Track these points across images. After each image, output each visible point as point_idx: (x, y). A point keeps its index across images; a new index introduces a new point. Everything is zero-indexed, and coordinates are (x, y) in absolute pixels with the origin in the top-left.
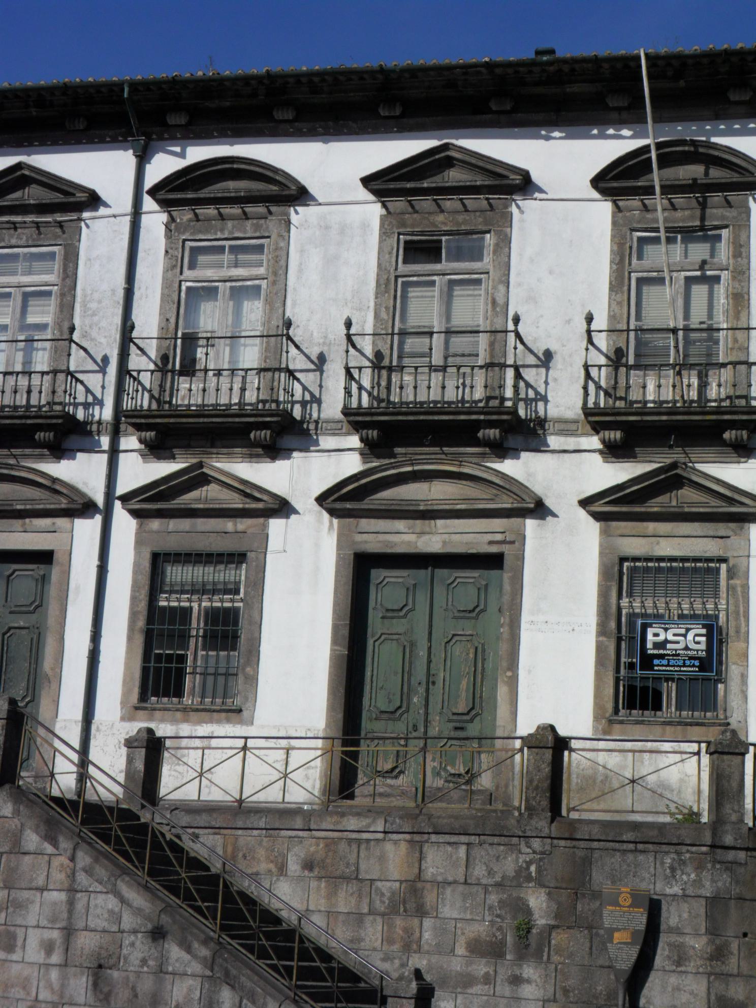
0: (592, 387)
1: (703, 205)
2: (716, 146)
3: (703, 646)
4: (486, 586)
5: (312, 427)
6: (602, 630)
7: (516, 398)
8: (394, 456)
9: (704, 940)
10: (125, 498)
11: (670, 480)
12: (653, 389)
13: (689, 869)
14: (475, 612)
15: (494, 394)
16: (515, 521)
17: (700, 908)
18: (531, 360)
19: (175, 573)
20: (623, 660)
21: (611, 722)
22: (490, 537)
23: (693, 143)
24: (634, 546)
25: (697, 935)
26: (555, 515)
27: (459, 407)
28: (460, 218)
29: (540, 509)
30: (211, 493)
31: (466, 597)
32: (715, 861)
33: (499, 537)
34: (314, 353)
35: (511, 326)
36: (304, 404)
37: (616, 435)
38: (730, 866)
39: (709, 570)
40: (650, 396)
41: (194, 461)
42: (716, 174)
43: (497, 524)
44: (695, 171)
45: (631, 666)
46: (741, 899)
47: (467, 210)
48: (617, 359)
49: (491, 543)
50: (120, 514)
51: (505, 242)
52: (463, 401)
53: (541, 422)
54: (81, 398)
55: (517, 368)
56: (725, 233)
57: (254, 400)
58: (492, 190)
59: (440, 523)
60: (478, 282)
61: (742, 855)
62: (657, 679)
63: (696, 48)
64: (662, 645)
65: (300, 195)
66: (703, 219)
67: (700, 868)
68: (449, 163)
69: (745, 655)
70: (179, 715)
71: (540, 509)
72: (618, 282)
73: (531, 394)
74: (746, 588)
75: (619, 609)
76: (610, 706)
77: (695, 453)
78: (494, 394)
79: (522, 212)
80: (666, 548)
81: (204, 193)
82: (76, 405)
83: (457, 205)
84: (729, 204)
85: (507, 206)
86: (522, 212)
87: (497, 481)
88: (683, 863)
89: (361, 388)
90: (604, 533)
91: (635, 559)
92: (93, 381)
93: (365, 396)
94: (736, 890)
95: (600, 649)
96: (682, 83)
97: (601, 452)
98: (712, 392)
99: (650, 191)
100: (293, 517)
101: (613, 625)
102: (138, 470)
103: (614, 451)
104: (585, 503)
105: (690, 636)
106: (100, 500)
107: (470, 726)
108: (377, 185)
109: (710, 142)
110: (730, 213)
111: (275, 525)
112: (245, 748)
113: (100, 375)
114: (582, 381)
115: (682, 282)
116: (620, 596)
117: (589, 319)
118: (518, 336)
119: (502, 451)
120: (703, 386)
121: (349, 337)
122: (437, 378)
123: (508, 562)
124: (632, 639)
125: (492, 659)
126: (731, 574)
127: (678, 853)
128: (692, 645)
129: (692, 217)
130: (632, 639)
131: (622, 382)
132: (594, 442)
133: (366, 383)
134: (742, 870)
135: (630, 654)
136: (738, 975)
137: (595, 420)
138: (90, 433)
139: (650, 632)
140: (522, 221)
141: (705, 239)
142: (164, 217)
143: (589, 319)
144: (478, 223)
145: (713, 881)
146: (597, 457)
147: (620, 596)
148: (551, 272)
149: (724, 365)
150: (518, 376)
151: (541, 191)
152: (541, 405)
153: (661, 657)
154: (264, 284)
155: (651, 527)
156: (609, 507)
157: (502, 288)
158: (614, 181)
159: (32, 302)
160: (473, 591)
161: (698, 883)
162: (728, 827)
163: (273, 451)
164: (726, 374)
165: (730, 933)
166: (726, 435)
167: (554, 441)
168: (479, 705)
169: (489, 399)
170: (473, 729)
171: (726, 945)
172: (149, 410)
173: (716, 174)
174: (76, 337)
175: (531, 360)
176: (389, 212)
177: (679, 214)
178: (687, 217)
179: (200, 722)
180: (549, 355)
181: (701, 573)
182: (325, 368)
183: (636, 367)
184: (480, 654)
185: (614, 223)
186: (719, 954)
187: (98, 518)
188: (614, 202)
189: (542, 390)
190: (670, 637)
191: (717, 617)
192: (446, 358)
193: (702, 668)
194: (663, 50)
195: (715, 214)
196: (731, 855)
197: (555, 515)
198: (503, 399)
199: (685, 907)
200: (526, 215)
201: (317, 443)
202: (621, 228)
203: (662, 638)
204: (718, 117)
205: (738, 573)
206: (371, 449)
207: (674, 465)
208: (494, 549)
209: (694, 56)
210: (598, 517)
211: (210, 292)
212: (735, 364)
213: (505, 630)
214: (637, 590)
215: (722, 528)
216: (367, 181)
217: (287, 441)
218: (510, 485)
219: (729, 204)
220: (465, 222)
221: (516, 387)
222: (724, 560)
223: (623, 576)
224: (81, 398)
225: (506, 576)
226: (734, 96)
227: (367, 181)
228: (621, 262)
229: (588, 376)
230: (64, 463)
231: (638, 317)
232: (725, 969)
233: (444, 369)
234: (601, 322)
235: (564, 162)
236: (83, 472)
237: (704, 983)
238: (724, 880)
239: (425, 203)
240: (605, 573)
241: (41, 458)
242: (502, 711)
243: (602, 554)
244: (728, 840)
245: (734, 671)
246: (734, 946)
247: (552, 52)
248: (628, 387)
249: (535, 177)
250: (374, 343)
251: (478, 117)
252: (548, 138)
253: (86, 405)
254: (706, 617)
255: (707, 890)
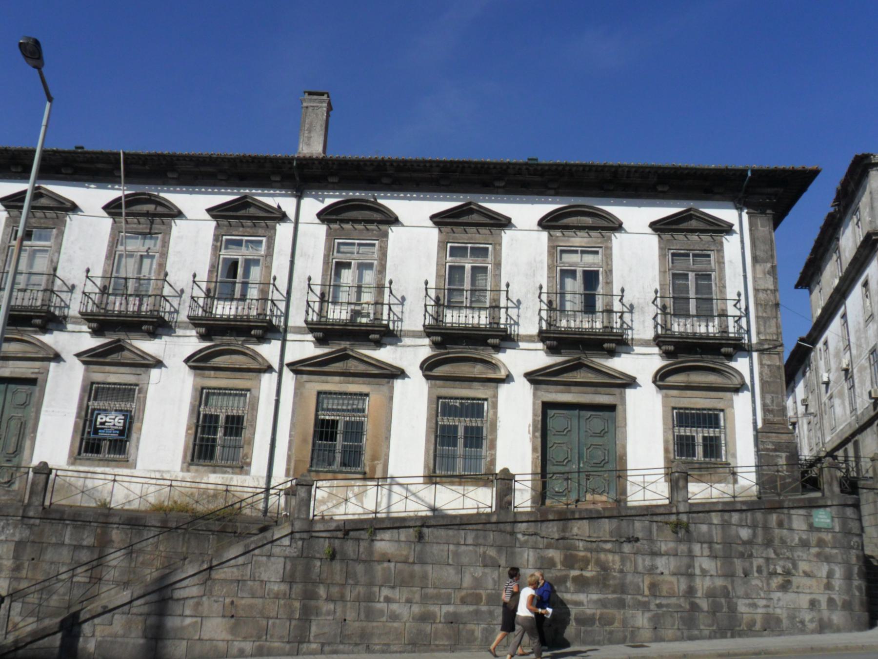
0: (427, 315)
1: (152, 223)
2: (158, 196)
3: (122, 425)
4: (31, 394)
5: (173, 325)
6: (78, 416)
7: (389, 320)
8: (446, 349)
9: (11, 561)
10: (288, 365)
11: (117, 347)
12: (117, 305)
13: (10, 527)
14: (24, 405)
15: (608, 328)
16: (46, 363)
17: (12, 546)
18: (65, 289)
19: (328, 403)
20: (199, 435)
21: (76, 459)
22: (32, 370)
23: (149, 195)
24: (98, 377)
25: (8, 559)
26: (64, 361)
27: (592, 333)
28: (42, 221)
29: (57, 358)
30: (353, 366)
31: (21, 398)
32: (23, 524)
33: (36, 370)
34: (178, 290)
35: (272, 282)
36: (394, 322)
37: (438, 339)
38: (31, 527)
39: (241, 395)
40: (116, 309)
41: (577, 356)
42: (160, 209)
43: (38, 364)
44: (150, 208)
45: (89, 433)
46: (33, 542)
47: (46, 217)
48: (104, 291)
49: (33, 373)
50: (286, 371)
51: (61, 233)
52: (592, 328)
53: (65, 318)
54: (168, 309)
55: (389, 305)
56: (160, 236)
57: (255, 313)
58: (492, 225)
59: (11, 362)
60: (47, 251)
61: (37, 521)
62: (100, 440)
63: (146, 152)
64: (103, 424)
65: (179, 214)
66: (151, 229)
67: (15, 527)
68: (471, 211)
69: (140, 429)
70: (96, 462)
71: (57, 358)
72: (111, 254)
73: (396, 318)
74: (145, 398)
75: (88, 406)
76: (76, 451)
77: (132, 335)
78: (608, 328)
79: (71, 220)
80: (112, 379)
81: (461, 220)
82: (165, 312)
83: (136, 220)
84: (163, 223)
85: (64, 217)
86: (71, 220)
87: (38, 344)
88: (8, 525)
89: (314, 311)
90: (86, 370)
91: (98, 383)
92: (175, 302)
93: (315, 315)
94: (32, 538)
95: (76, 424)
96: (147, 167)
97: (90, 333)
98: (144, 308)
99: (120, 214)
100: (406, 379)
101: (83, 413)
102: (90, 342)
103: (96, 332)
104: (78, 355)
105: (116, 420)
106: (276, 366)
107: (14, 460)
108: (214, 213)
109: (375, 202)
110: (163, 227)
111: (629, 392)
112: (114, 481)
113: (516, 310)
114: (423, 313)
115: (138, 257)
116: (89, 400)
117: (426, 283)
118: (274, 285)
119: (44, 330)
120: (141, 305)
121: (309, 285)
122: (20, 294)
123: (39, 382)
124: (91, 421)
125: (26, 429)
126: (139, 392)
127: (7, 520)
128: (117, 424)
129: (146, 228)
130: (91, 421)
131: (104, 301)
132: (194, 333)
133: (201, 304)
134: (36, 528)
135: (90, 427)
136: (26, 578)
137: (543, 336)
138: (171, 327)
139: (99, 417)
140: (70, 224)
141: (151, 238)
142: (214, 223)
143: (426, 283)
144: (50, 223)
145: (20, 533)
146: (88, 335)
147: (89, 400)
148: (80, 249)
149: (150, 296)
150: (390, 309)
151: (82, 211)
152: (66, 310)
153: (102, 429)
154: (375, 262)
155: (107, 368)
156: (535, 378)
157: (56, 255)
158: (112, 208)
159: (38, 255)
160: (24, 395)
161: (13, 534)
162: (32, 508)
163: (153, 335)
164: (151, 299)
165: (25, 558)
166: (253, 332)
167: (70, 327)
168: (18, 450)
169: (259, 315)
170: (15, 461)
171: (22, 564)
172: (92, 311)
173: (160, 209)
174: (167, 279)
175: (65, 289)
176: (10, 216)
177: (141, 226)
178: (144, 228)
179: (98, 466)
180: (403, 298)
181: (475, 409)
182: (405, 303)
183: (113, 294)
184: (23, 425)
185: (112, 228)
186: (17, 568)
187: (275, 375)
188: (659, 236)
189: (68, 303)
190: (108, 420)
191: (131, 411)
192: (27, 285)
193: (120, 435)
194: (133, 151)
195: (157, 227)
196: (32, 521)
197: (64, 361)
198: (266, 315)
199: (6, 546)
200: (73, 222)
201: (175, 332)
202: (331, 236)
203: (104, 420)
204: (164, 184)
205: (143, 391)
206: (436, 345)
207: (119, 340)
208: (33, 376)
209: (144, 156)
210: (84, 363)
211: (348, 265)
212: (156, 296)
213: (33, 414)
214: (99, 397)
215: (138, 370)
216: (209, 211)
217: (160, 330)
218: (44, 346)
219: (163, 223)
220: (44, 223)
221: (389, 314)
222: (137, 385)
223: (93, 391)
224: (168, 309)
225: (37, 389)
226: (170, 175)
227: (209, 211)
228: (113, 246)
229: (308, 305)
230: (382, 350)
231: (118, 271)
232: (19, 575)
233: (25, 290)
234: (432, 284)
235: (91, 198)
236: (269, 351)
237: (7, 582)
238: (26, 533)
239: (680, 237)
240: (83, 389)
241: (36, 332)
242: (26, 452)
243: (84, 380)
244: (31, 514)
245: (134, 436)
246: (26, 564)
247: (82, 148)
248: (107, 304)
249: (513, 221)
250: (548, 297)
251: (57, 176)
252: (88, 187)
253: (170, 313)
254: (127, 411)
255: (17, 538)
